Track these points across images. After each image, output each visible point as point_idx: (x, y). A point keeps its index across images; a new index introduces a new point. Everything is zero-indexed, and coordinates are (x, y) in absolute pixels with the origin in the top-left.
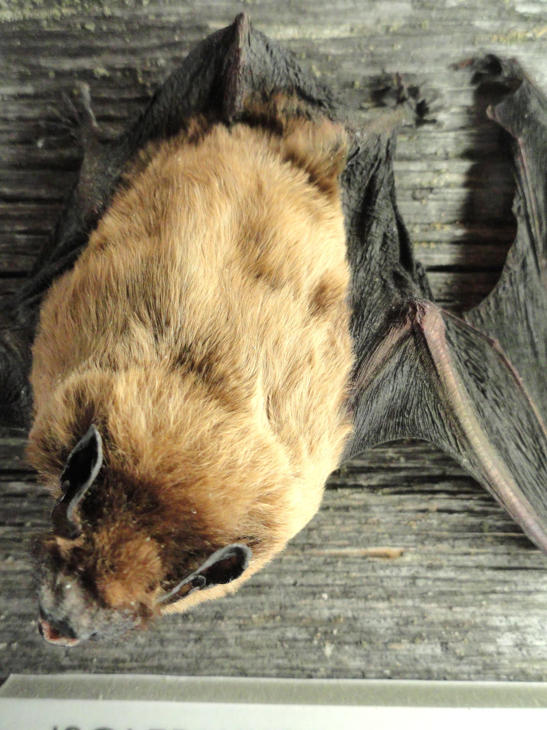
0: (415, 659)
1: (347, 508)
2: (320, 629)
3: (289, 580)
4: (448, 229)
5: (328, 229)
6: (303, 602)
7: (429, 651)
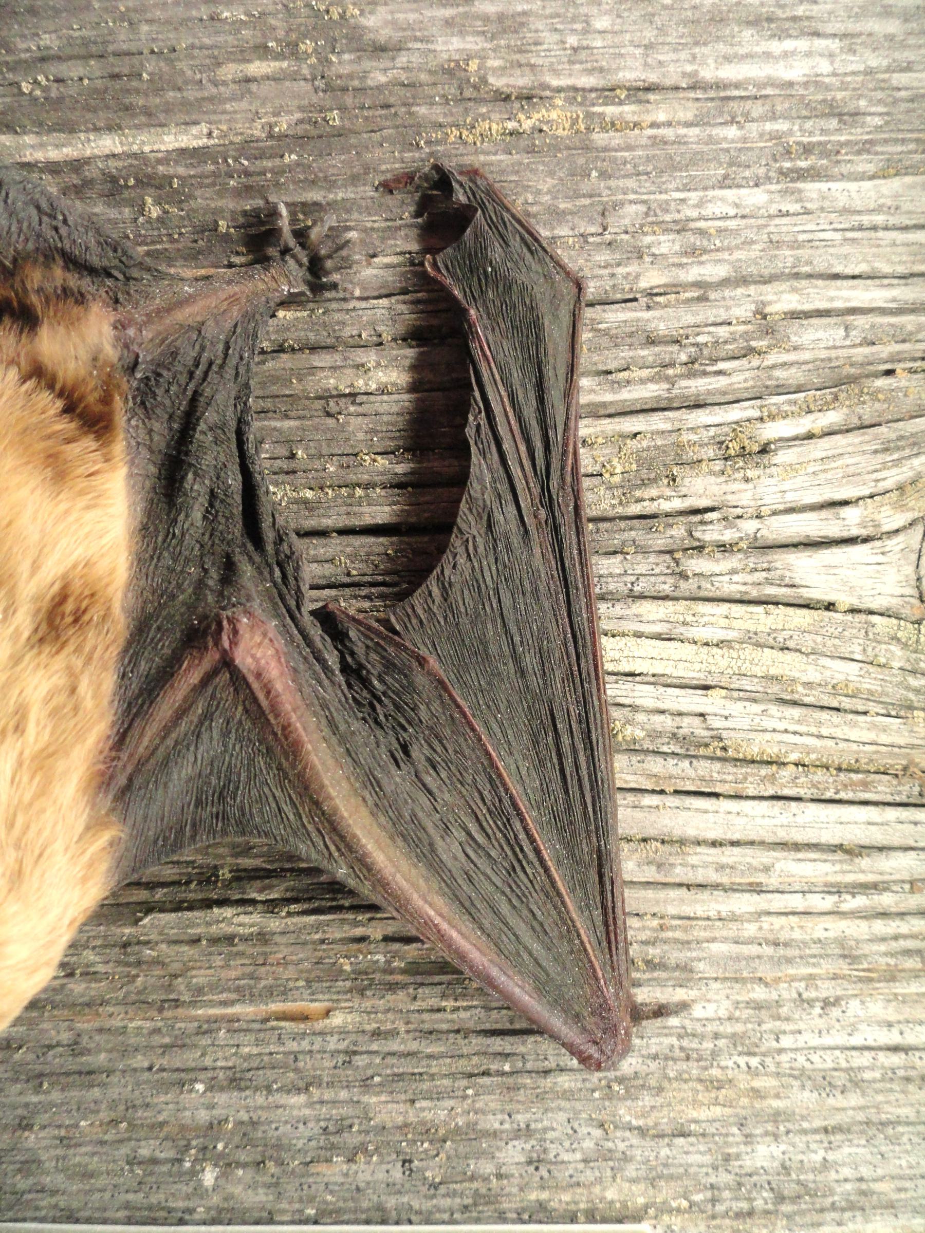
0: (358, 1189)
1: (230, 939)
2: (194, 1143)
3: (140, 1061)
4: (382, 462)
5: (82, 493)
6: (163, 1098)
7: (381, 1176)
